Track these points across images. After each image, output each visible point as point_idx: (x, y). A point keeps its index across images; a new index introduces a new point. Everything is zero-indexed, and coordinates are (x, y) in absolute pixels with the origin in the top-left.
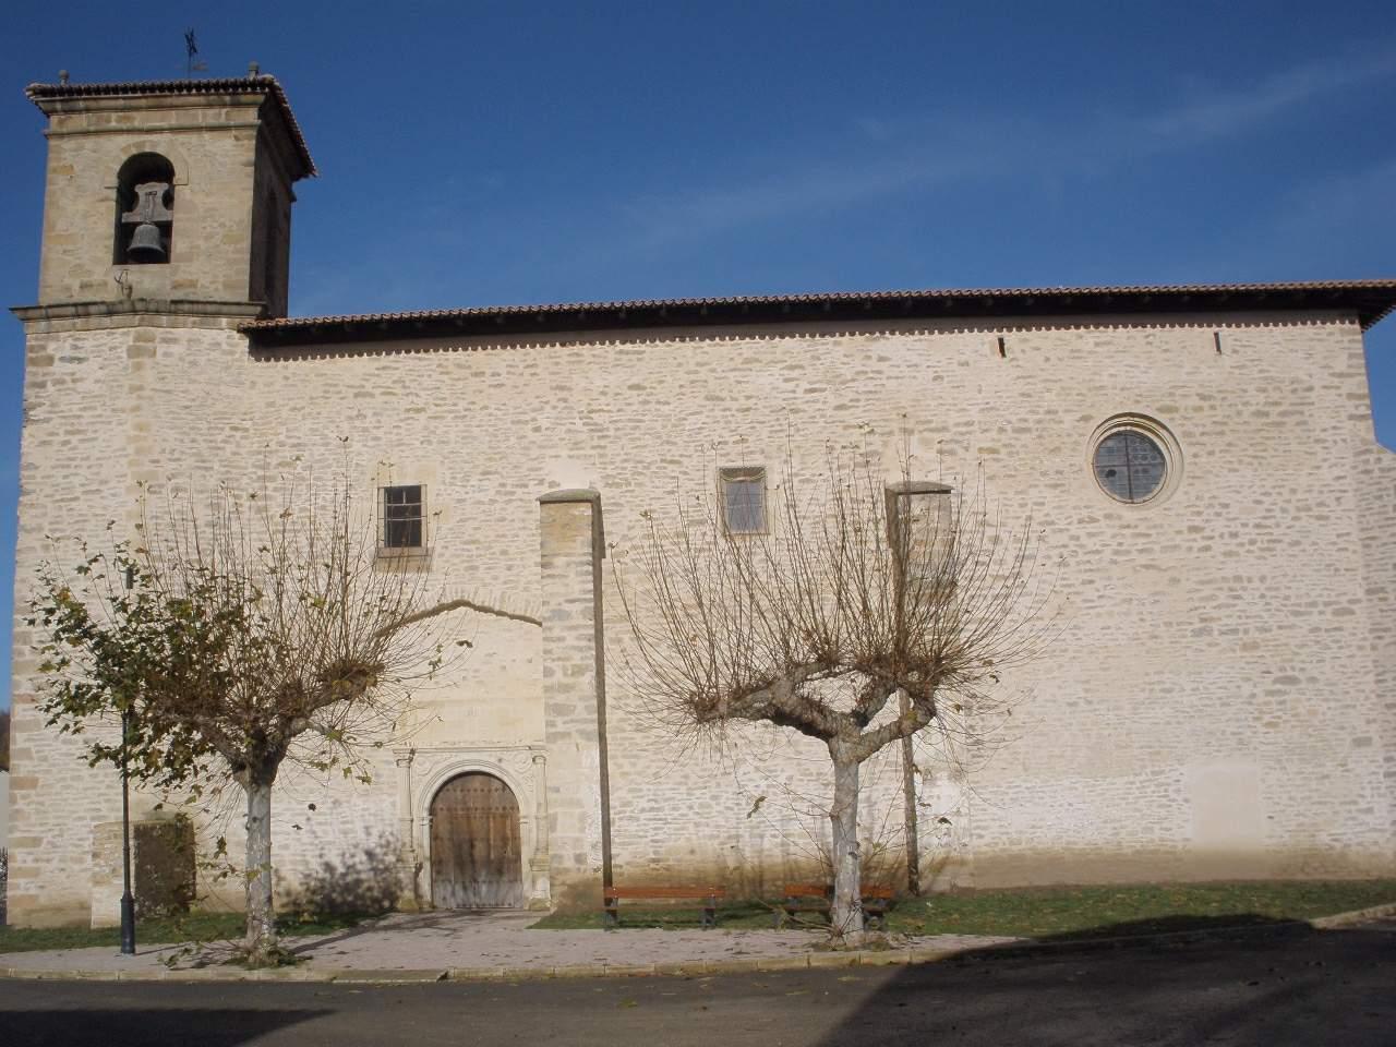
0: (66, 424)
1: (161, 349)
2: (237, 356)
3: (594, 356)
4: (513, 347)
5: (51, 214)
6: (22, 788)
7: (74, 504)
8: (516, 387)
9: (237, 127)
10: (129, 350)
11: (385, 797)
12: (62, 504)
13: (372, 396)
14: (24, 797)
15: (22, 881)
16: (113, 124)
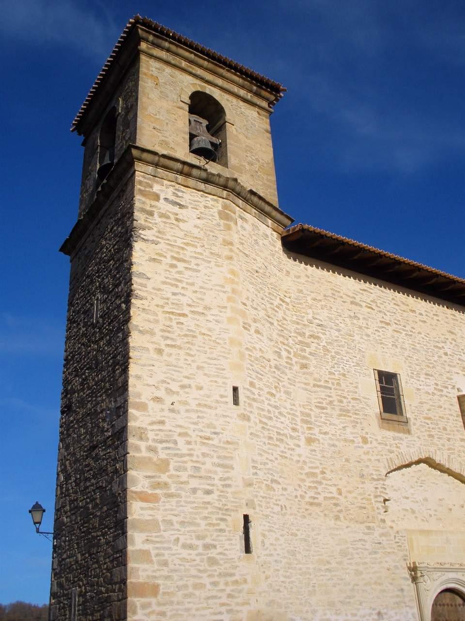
4: (426, 301)
6: (142, 595)
7: (182, 319)
12: (171, 316)
14: (144, 606)
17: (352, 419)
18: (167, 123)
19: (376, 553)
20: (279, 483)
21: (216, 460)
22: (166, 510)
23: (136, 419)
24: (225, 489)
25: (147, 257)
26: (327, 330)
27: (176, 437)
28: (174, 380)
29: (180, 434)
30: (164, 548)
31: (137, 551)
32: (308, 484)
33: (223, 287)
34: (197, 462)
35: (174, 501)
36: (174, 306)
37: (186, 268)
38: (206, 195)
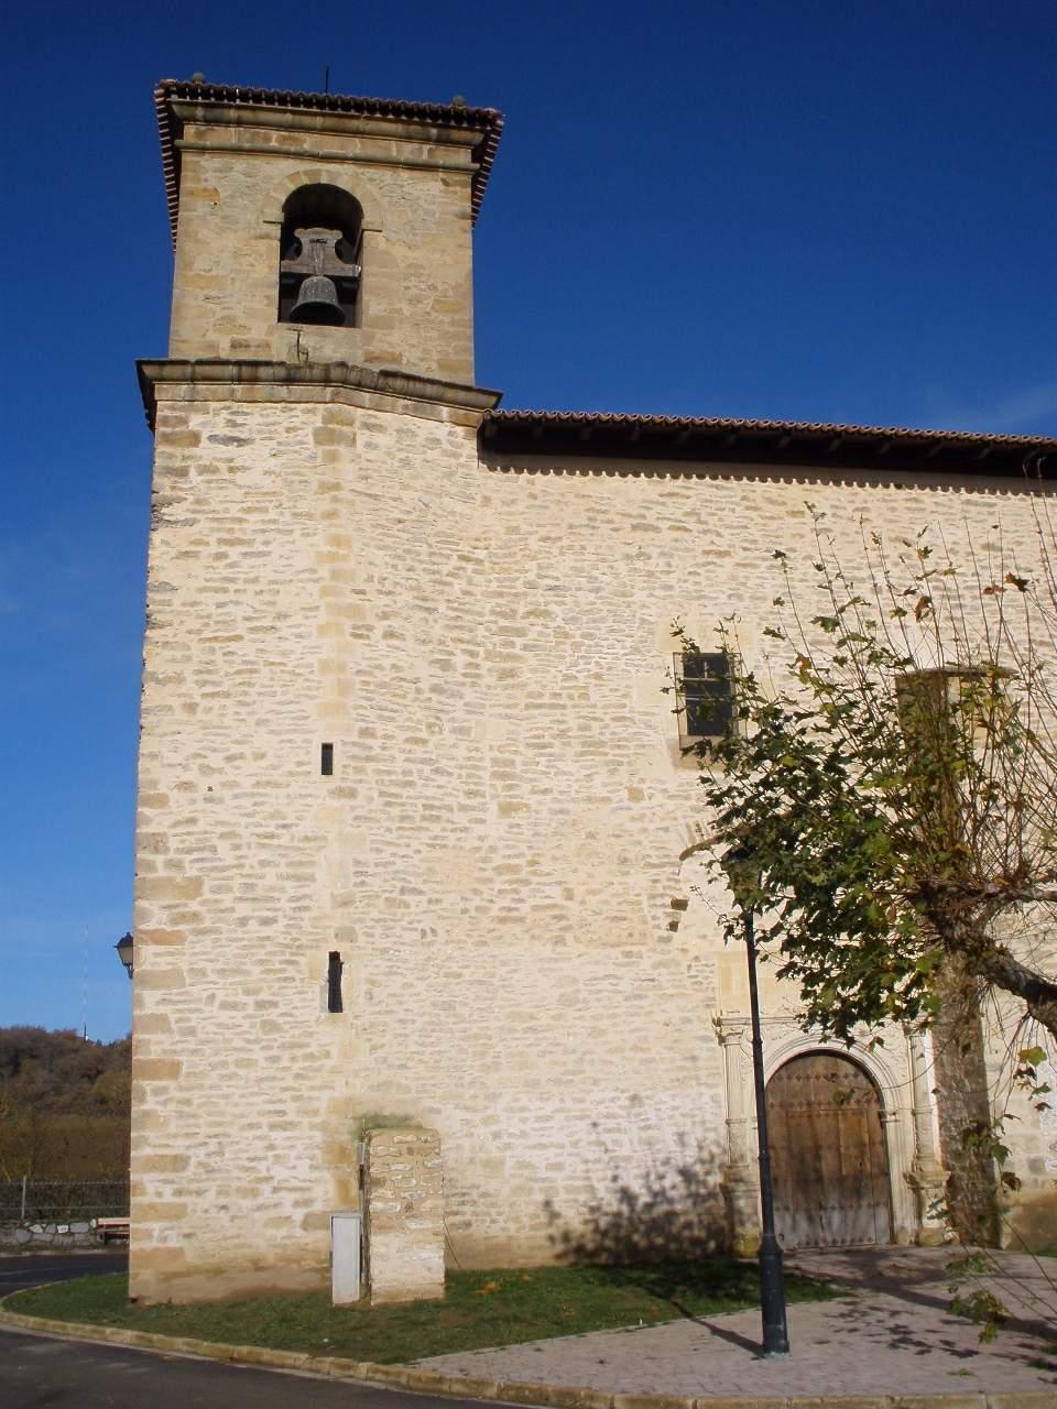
0: (219, 530)
1: (363, 437)
2: (463, 460)
3: (936, 503)
4: (837, 483)
5: (185, 247)
6: (153, 1077)
7: (233, 646)
8: (847, 534)
9: (446, 168)
10: (317, 433)
11: (703, 1089)
12: (214, 644)
13: (657, 529)
14: (156, 1092)
15: (156, 1227)
16: (274, 144)
17: (610, 757)
18: (233, 279)
19: (639, 997)
20: (421, 893)
21: (284, 870)
22: (194, 954)
23: (148, 821)
24: (297, 914)
25: (173, 553)
26: (568, 594)
27: (215, 841)
28: (214, 750)
29: (222, 836)
30: (190, 1011)
31: (146, 1016)
32: (497, 886)
33: (313, 571)
34: (249, 876)
35: (208, 939)
36: (220, 626)
37: (245, 554)
38: (293, 405)
